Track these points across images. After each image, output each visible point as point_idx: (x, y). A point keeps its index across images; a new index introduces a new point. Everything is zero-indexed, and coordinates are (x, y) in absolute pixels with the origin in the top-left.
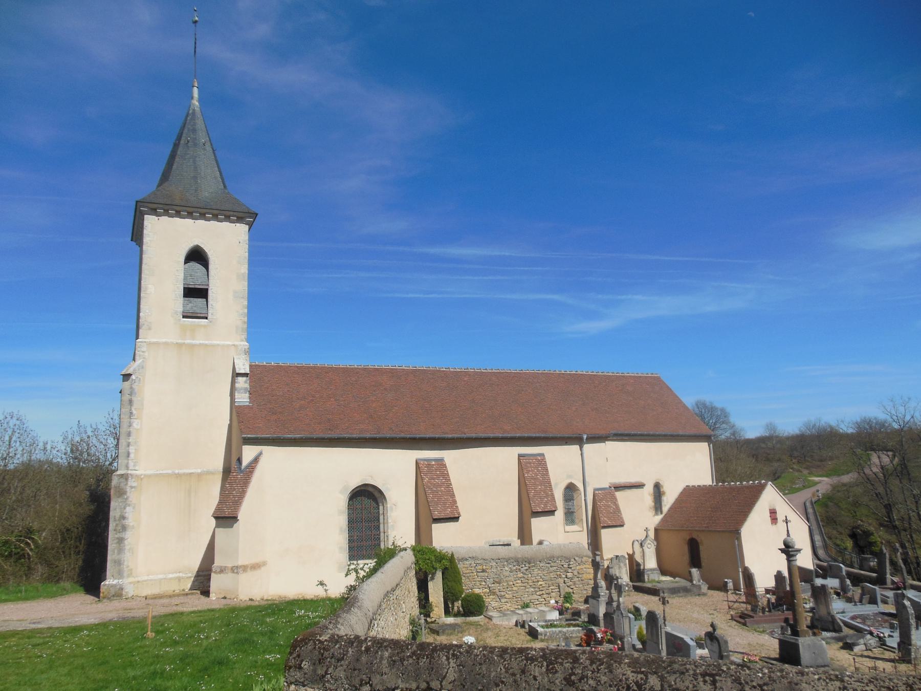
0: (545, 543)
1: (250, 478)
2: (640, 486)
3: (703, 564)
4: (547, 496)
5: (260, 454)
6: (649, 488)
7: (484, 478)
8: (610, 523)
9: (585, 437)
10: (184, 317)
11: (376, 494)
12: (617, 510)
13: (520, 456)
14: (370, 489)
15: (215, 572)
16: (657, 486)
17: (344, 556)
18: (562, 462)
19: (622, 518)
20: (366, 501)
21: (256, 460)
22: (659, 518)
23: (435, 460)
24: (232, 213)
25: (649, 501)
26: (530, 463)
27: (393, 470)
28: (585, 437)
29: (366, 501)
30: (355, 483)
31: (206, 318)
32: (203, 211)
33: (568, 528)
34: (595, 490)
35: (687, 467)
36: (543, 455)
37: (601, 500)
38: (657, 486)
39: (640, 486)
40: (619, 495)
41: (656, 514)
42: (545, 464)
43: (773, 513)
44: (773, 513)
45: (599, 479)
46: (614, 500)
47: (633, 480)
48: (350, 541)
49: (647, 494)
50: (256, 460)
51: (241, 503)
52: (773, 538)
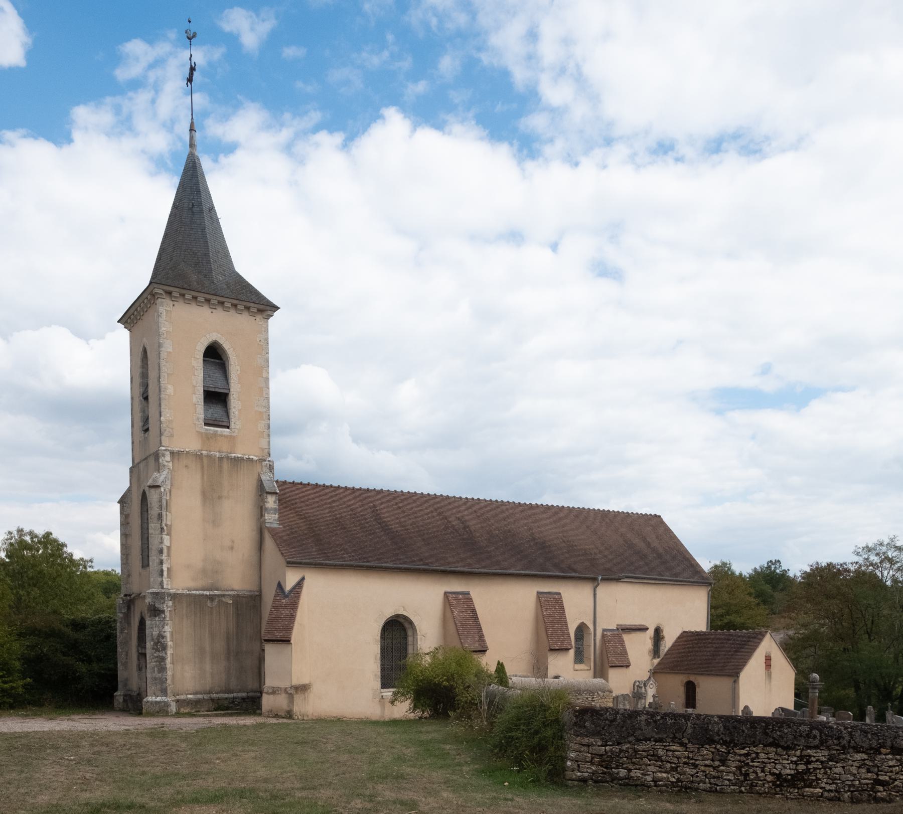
0: (561, 678)
1: (297, 603)
2: (644, 629)
3: (697, 705)
4: (564, 634)
5: (303, 579)
6: (651, 632)
7: (506, 612)
8: (617, 663)
9: (600, 578)
10: (206, 424)
11: (406, 625)
12: (624, 652)
13: (446, 593)
14: (402, 621)
15: (267, 693)
16: (658, 631)
17: (377, 684)
18: (577, 601)
19: (628, 659)
20: (396, 630)
21: (300, 584)
22: (656, 661)
23: (462, 593)
24: (252, 305)
25: (649, 645)
26: (548, 601)
27: (422, 601)
28: (600, 578)
29: (396, 630)
30: (389, 613)
31: (228, 427)
32: (235, 302)
33: (578, 667)
34: (604, 630)
35: (685, 612)
36: (559, 594)
37: (609, 641)
38: (658, 631)
39: (644, 629)
40: (627, 638)
41: (654, 658)
42: (562, 603)
43: (768, 659)
44: (768, 659)
45: (608, 622)
46: (622, 642)
47: (637, 622)
48: (383, 669)
49: (646, 640)
50: (300, 584)
51: (292, 628)
52: (765, 685)
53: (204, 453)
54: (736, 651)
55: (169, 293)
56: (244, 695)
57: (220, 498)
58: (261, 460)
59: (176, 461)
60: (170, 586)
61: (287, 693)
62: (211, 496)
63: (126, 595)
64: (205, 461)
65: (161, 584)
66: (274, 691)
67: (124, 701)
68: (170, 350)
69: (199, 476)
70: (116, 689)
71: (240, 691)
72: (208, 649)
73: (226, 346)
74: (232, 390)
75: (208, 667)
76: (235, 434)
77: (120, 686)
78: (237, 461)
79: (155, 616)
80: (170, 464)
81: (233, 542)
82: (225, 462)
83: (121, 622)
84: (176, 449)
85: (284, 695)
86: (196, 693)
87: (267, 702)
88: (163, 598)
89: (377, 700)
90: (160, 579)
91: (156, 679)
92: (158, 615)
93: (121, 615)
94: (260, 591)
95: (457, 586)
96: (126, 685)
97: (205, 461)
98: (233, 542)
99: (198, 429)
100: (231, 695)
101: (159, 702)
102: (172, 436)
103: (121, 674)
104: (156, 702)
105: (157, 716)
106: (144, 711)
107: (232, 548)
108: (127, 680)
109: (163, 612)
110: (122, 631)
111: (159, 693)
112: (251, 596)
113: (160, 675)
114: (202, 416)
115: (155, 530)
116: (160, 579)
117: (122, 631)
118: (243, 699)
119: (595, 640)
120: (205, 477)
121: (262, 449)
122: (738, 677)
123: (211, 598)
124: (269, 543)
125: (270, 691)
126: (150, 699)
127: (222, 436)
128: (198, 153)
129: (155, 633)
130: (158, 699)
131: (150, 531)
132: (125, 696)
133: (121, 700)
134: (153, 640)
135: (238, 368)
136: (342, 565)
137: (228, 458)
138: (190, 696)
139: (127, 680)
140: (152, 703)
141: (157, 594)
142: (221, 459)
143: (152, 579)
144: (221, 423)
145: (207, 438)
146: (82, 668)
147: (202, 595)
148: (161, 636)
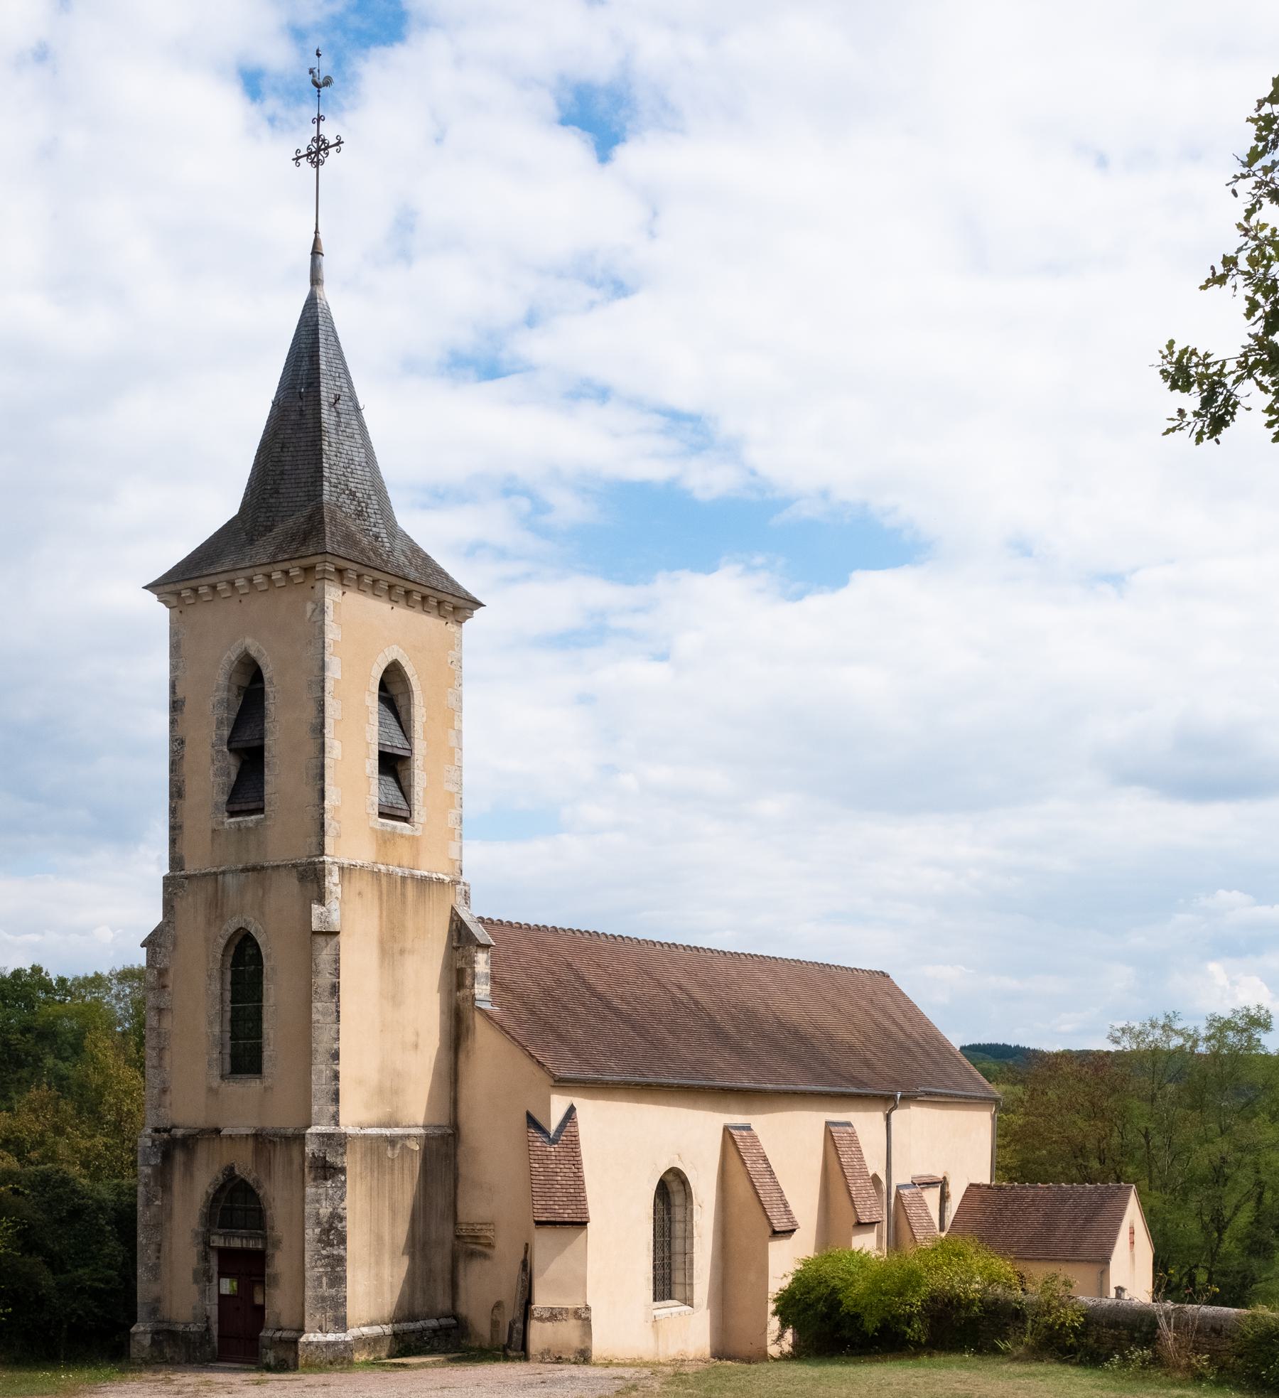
10: (382, 815)
15: (541, 1319)
31: (405, 820)
32: (342, 564)
36: (849, 1124)
53: (383, 868)
54: (1088, 1220)
55: (340, 572)
56: (433, 1323)
57: (402, 952)
58: (455, 883)
59: (346, 883)
60: (348, 1125)
61: (579, 1318)
62: (391, 948)
63: (157, 1130)
64: (384, 881)
65: (335, 1118)
66: (554, 1315)
67: (154, 1343)
68: (338, 676)
69: (376, 912)
70: (134, 1320)
71: (427, 1317)
72: (387, 1237)
73: (409, 670)
74: (416, 751)
75: (386, 1272)
76: (418, 834)
77: (141, 1312)
78: (424, 882)
79: (326, 1179)
80: (339, 889)
81: (417, 1034)
82: (409, 881)
83: (146, 1185)
84: (346, 862)
85: (573, 1322)
86: (371, 1324)
87: (539, 1335)
88: (343, 1145)
89: (650, 1324)
90: (332, 1109)
91: (323, 1299)
92: (332, 1176)
93: (148, 1170)
94: (455, 1125)
95: (738, 1119)
96: (154, 1311)
97: (384, 881)
98: (417, 1034)
99: (372, 824)
100: (419, 1325)
101: (335, 1344)
102: (338, 836)
103: (145, 1288)
104: (328, 1345)
105: (328, 1371)
106: (301, 1361)
107: (416, 1046)
108: (158, 1300)
109: (343, 1170)
110: (148, 1203)
111: (330, 1325)
112: (442, 1136)
113: (333, 1291)
114: (376, 800)
115: (324, 1014)
116: (332, 1109)
117: (148, 1203)
118: (434, 1330)
119: (888, 1204)
120: (385, 914)
121: (452, 861)
122: (1108, 1263)
123: (392, 1141)
124: (484, 1039)
125: (547, 1315)
126: (311, 1337)
127: (402, 836)
128: (330, 295)
129: (325, 1211)
130: (331, 1337)
131: (315, 1017)
132: (156, 1333)
133: (147, 1341)
134: (319, 1223)
135: (424, 710)
136: (637, 1084)
137: (413, 877)
138: (365, 1330)
139: (158, 1300)
140: (318, 1345)
141: (330, 1136)
142: (404, 878)
143: (315, 1108)
144: (399, 813)
145: (385, 840)
146: (47, 1280)
147: (381, 1136)
148: (337, 1217)
